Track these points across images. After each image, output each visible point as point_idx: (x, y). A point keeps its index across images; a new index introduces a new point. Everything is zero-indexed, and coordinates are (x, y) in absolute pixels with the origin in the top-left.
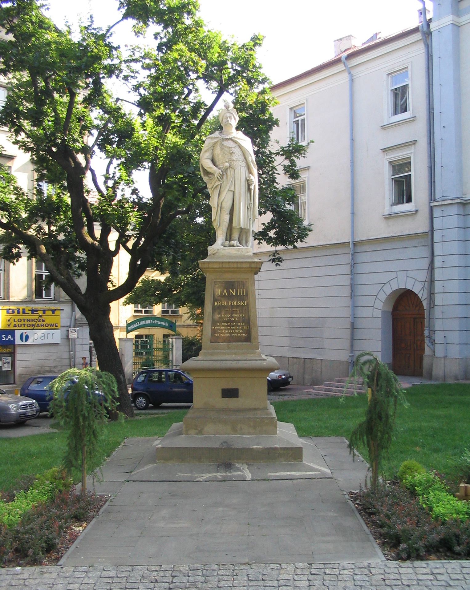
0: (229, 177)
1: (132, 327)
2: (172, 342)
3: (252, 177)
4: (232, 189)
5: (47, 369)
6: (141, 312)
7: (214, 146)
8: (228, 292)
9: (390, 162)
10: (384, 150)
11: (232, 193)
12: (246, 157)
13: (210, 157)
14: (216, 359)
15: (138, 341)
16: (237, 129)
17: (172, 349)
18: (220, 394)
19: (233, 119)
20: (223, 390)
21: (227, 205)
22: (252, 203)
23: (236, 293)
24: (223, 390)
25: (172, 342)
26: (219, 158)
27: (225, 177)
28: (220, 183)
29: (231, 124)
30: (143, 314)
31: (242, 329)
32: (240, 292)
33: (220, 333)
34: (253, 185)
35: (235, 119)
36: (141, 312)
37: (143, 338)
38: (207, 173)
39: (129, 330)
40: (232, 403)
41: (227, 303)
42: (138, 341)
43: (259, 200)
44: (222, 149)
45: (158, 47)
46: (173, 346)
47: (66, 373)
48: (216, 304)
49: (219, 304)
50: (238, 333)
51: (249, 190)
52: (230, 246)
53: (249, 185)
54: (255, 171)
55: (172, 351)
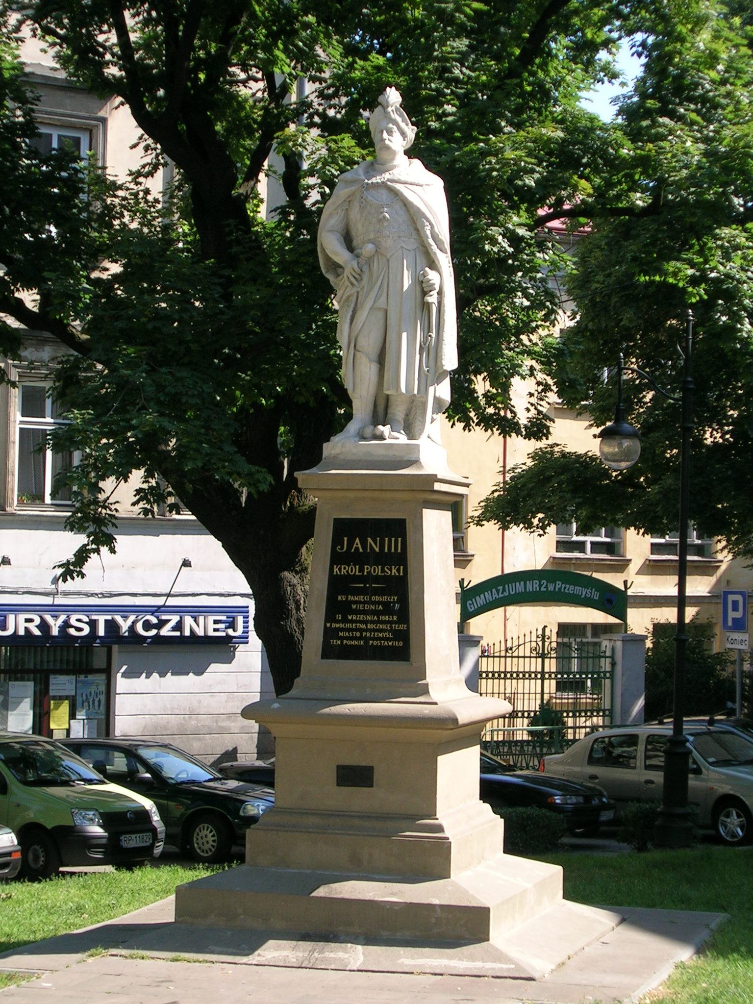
1: (480, 600)
2: (613, 649)
3: (432, 275)
4: (381, 303)
5: (206, 721)
6: (580, 546)
7: (349, 201)
11: (381, 315)
15: (568, 646)
16: (410, 153)
17: (612, 672)
18: (332, 776)
19: (397, 135)
20: (340, 768)
24: (340, 768)
25: (613, 649)
26: (359, 232)
27: (365, 277)
30: (589, 555)
33: (342, 638)
35: (403, 134)
36: (580, 546)
37: (584, 635)
38: (336, 267)
39: (471, 609)
40: (357, 798)
41: (361, 570)
42: (568, 646)
44: (362, 209)
46: (613, 664)
48: (336, 570)
50: (380, 639)
55: (612, 678)
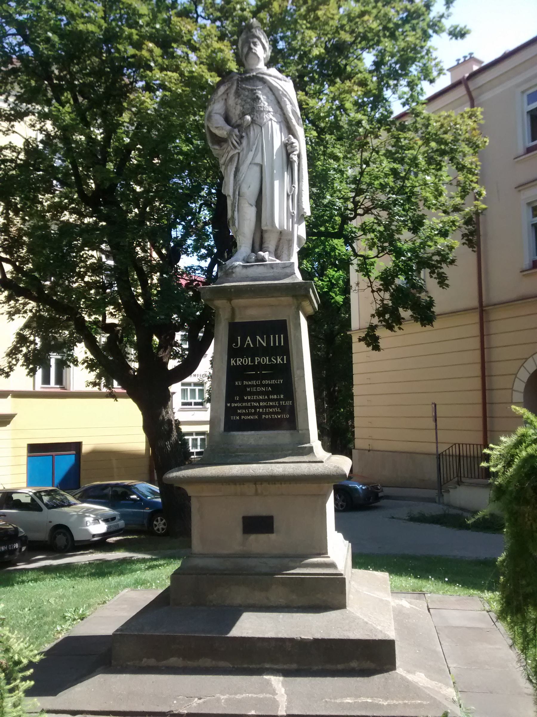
0: (252, 139)
4: (258, 160)
8: (254, 340)
9: (529, 204)
10: (521, 187)
11: (257, 169)
12: (283, 104)
13: (222, 111)
14: (307, 460)
21: (250, 190)
22: (296, 185)
23: (268, 343)
28: (237, 151)
29: (255, 54)
31: (280, 406)
32: (276, 340)
33: (240, 415)
34: (296, 153)
41: (253, 361)
43: (311, 185)
45: (423, 325)
47: (63, 495)
48: (233, 362)
49: (239, 363)
51: (289, 163)
52: (257, 260)
53: (288, 155)
54: (300, 130)
